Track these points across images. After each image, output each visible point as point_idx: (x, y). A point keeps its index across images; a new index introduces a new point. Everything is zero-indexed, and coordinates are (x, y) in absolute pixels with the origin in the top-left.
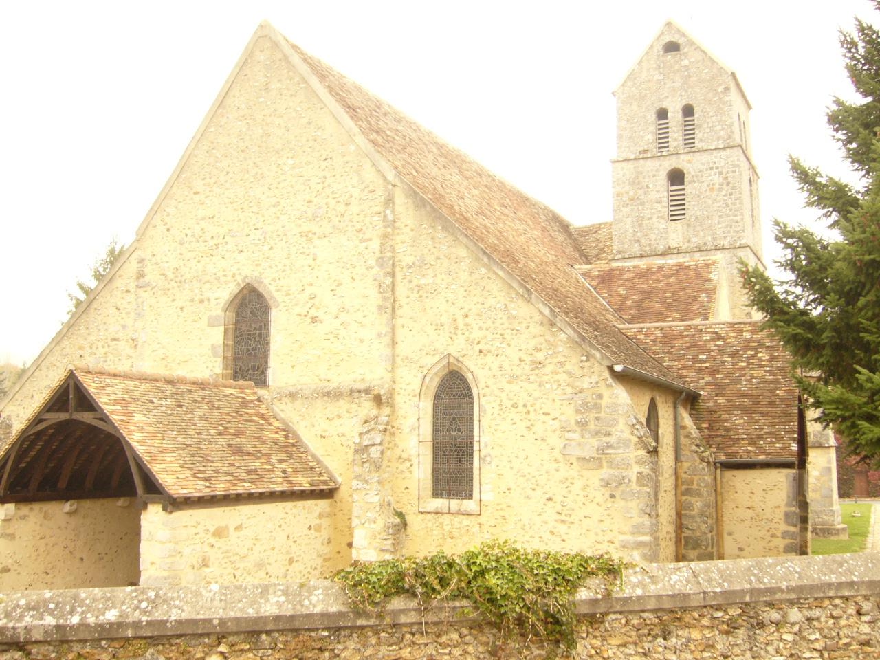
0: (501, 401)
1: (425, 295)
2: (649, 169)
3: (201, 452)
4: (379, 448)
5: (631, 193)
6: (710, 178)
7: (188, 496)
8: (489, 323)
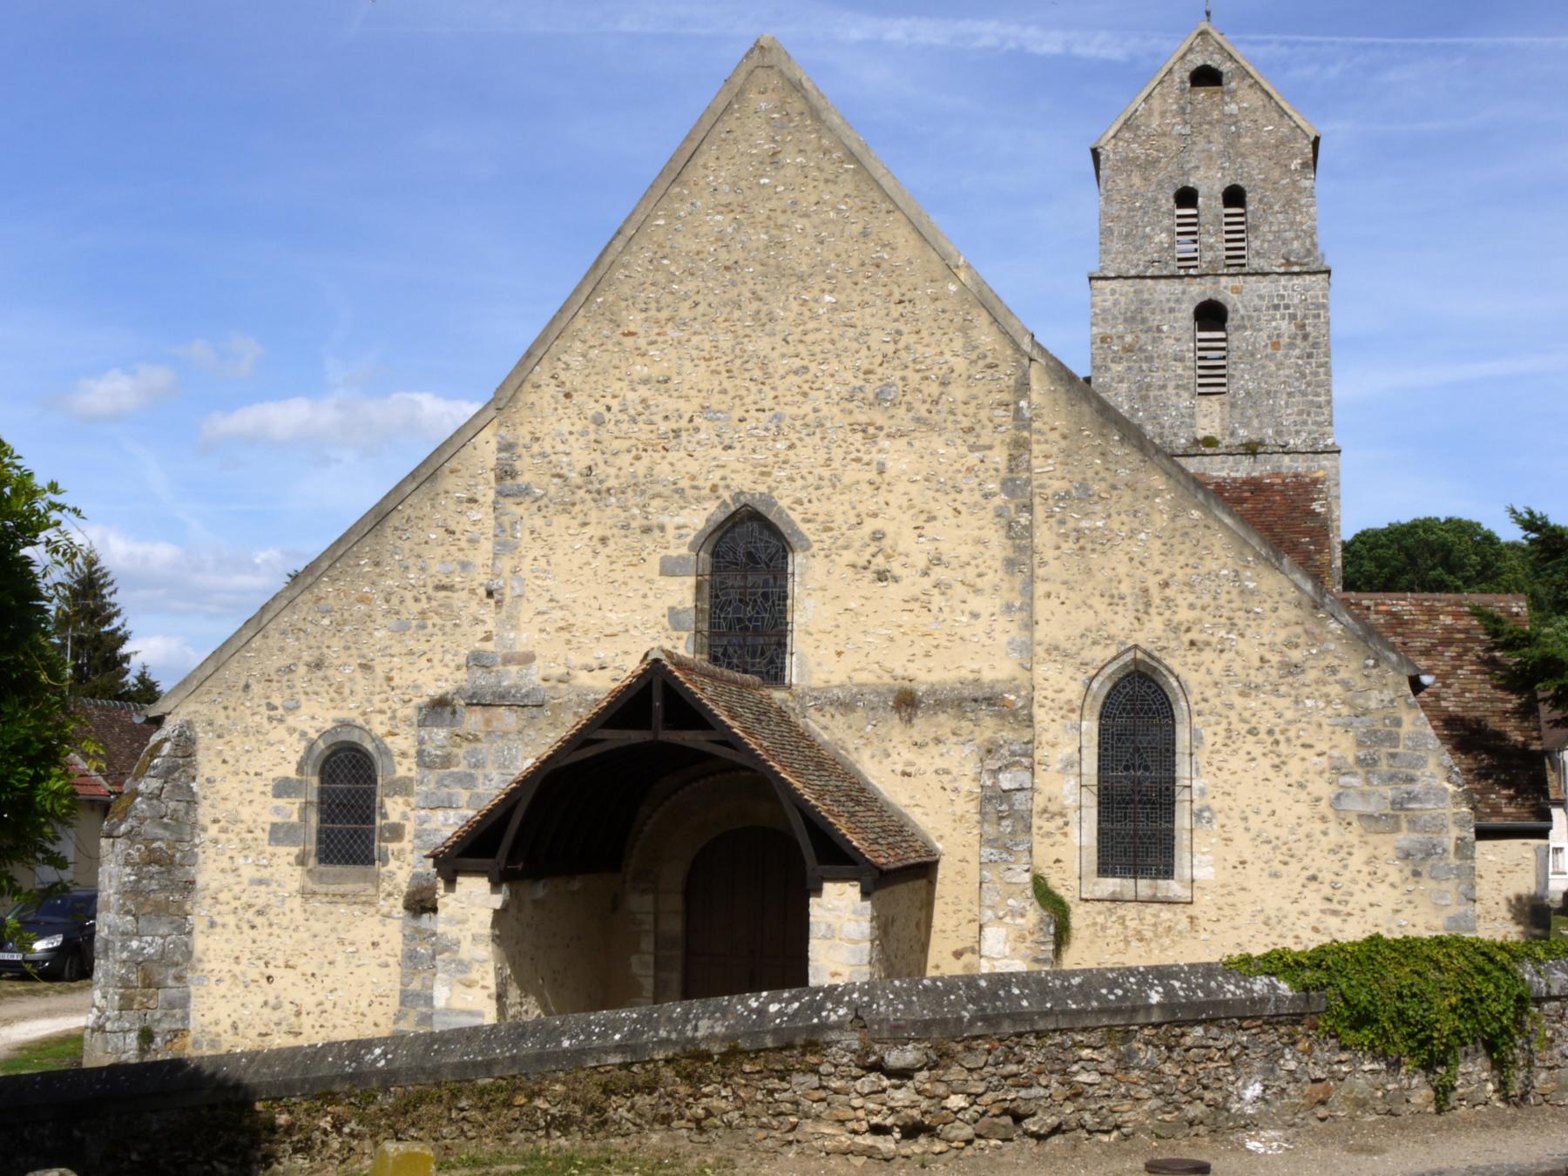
0: (1230, 724)
1: (1089, 546)
2: (1163, 298)
5: (1129, 339)
6: (1274, 324)
8: (1207, 599)
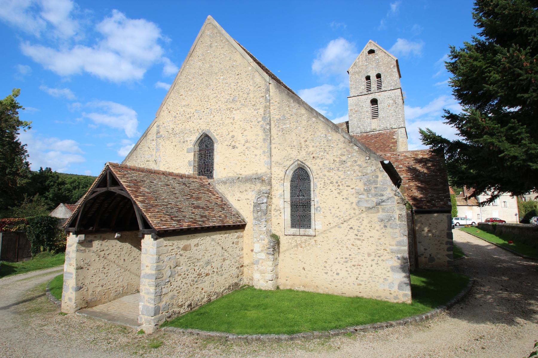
1: (285, 133)
3: (177, 207)
4: (265, 204)
7: (166, 229)
8: (317, 144)
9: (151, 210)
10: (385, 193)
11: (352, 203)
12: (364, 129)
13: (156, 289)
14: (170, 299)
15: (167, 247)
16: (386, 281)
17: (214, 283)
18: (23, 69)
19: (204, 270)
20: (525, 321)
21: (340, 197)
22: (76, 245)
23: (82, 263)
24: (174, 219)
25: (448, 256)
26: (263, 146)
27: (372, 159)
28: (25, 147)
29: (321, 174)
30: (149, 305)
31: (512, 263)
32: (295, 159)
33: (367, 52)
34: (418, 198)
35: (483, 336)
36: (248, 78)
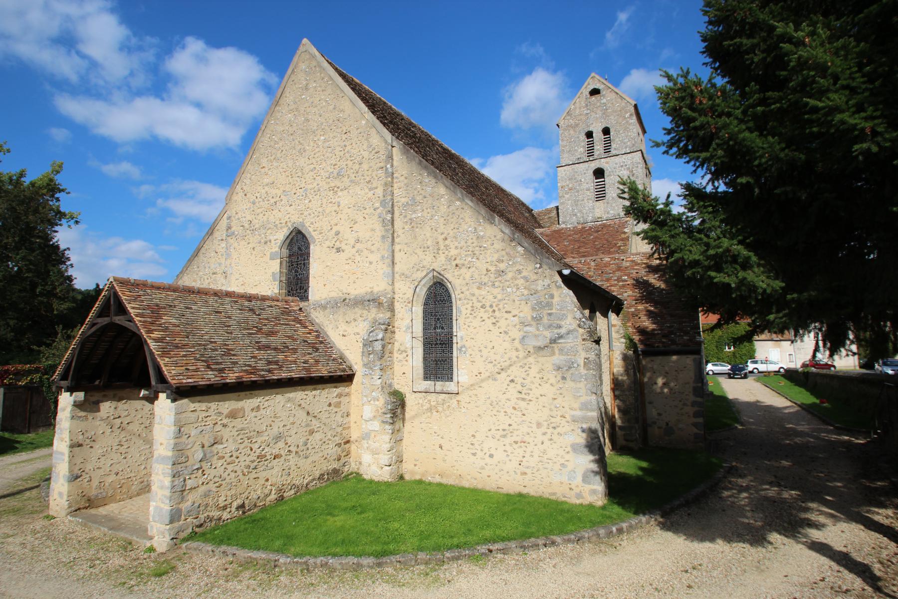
1: (415, 226)
4: (380, 342)
8: (463, 243)
9: (172, 353)
10: (563, 323)
11: (514, 340)
12: (583, 217)
13: (173, 481)
14: (201, 496)
15: (196, 414)
16: (564, 467)
17: (291, 471)
18: (59, 134)
19: (270, 450)
20: (786, 540)
21: (496, 331)
22: (69, 408)
23: (81, 437)
24: (213, 367)
25: (695, 425)
26: (382, 248)
27: (545, 267)
28: (67, 252)
29: (467, 293)
30: (162, 505)
31: (812, 437)
32: (428, 269)
33: (588, 93)
34: (648, 330)
35: (700, 565)
36: (360, 138)
